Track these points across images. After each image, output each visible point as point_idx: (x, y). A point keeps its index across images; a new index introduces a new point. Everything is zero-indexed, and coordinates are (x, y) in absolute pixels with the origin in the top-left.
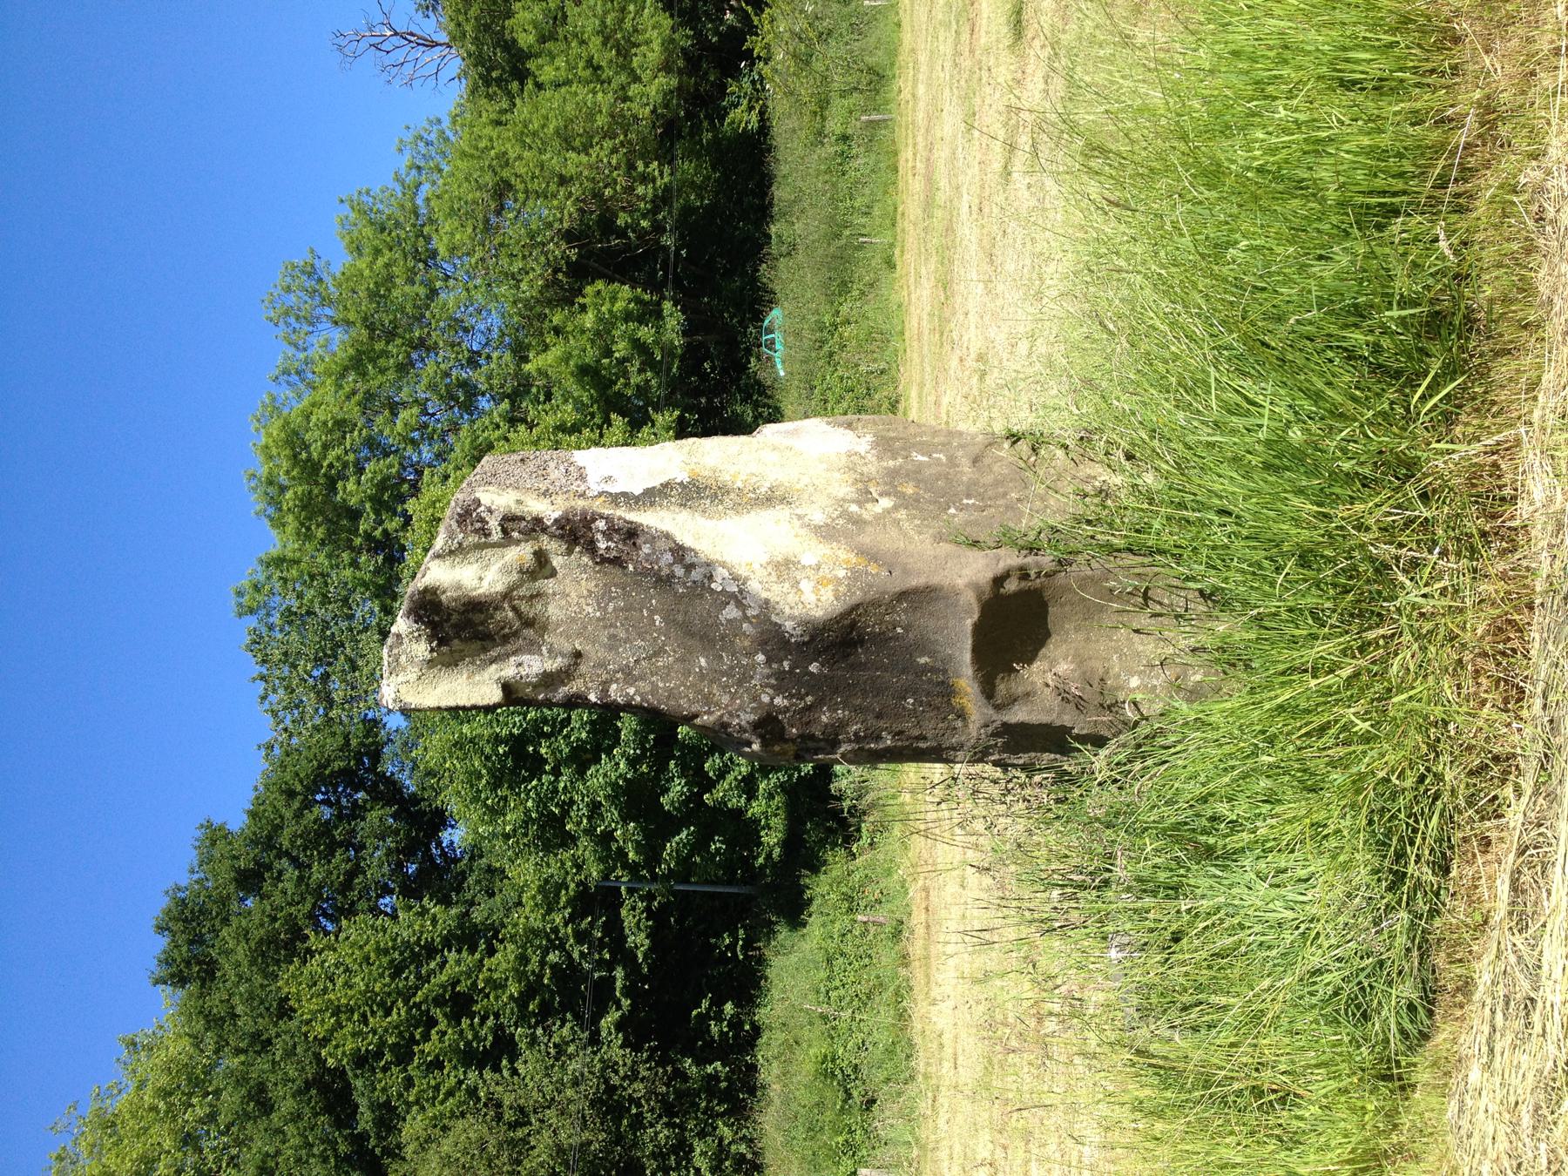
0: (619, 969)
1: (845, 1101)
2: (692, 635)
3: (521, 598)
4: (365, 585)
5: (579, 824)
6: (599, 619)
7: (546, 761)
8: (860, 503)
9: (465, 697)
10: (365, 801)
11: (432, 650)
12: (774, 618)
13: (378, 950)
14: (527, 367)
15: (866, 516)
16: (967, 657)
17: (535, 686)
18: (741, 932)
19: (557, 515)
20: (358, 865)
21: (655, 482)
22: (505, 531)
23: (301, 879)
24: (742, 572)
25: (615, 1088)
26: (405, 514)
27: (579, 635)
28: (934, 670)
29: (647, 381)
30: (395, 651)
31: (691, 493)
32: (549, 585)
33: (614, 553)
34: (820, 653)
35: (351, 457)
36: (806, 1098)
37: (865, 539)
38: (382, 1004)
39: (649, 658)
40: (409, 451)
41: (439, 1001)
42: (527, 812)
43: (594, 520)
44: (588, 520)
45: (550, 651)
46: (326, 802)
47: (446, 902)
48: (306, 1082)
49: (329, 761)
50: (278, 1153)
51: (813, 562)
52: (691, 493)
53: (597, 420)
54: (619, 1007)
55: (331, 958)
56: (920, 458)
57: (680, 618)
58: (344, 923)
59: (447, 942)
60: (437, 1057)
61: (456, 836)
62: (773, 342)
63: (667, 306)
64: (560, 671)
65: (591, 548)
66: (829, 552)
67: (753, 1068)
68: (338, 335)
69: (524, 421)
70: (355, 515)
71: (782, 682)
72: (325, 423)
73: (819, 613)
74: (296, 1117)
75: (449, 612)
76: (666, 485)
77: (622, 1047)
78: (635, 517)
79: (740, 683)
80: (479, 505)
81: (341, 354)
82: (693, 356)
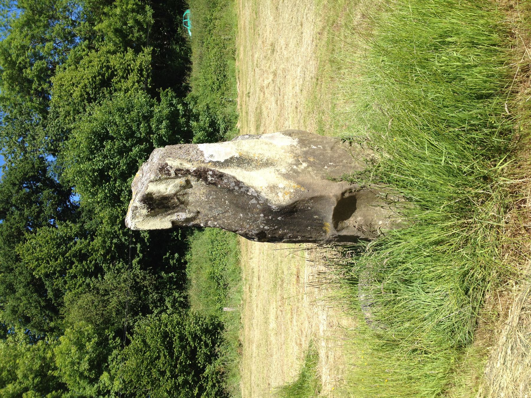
0: (139, 244)
1: (218, 286)
2: (239, 207)
3: (180, 195)
4: (36, 108)
5: (125, 198)
6: (206, 201)
7: (111, 177)
8: (297, 165)
9: (159, 226)
10: (41, 186)
11: (148, 212)
12: (269, 204)
13: (51, 239)
14: (95, 28)
15: (299, 170)
16: (331, 217)
17: (183, 222)
18: (180, 231)
19: (195, 169)
20: (41, 209)
21: (228, 157)
22: (176, 174)
23: (20, 214)
24: (259, 190)
25: (138, 283)
26: (50, 82)
27: (199, 206)
28: (319, 220)
29: (141, 36)
30: (135, 212)
31: (241, 161)
32: (189, 191)
33: (214, 182)
34: (282, 214)
35: (28, 60)
36: (204, 285)
37: (300, 179)
38: (54, 257)
39: (223, 213)
40: (50, 58)
41: (74, 256)
42: (106, 194)
43: (208, 171)
44: (206, 171)
45: (189, 211)
46: (27, 187)
47: (74, 222)
48: (28, 282)
49: (27, 173)
50: (19, 305)
51: (283, 186)
52: (241, 161)
53: (122, 49)
54: (139, 257)
55: (34, 241)
56: (314, 147)
57: (235, 202)
58: (38, 229)
59: (76, 235)
60: (75, 274)
61: (75, 198)
62: (186, 22)
63: (148, 7)
64: (192, 218)
65: (206, 179)
66: (288, 183)
67: (185, 274)
68: (20, 12)
69: (94, 48)
70: (30, 82)
71: (268, 222)
72: (17, 47)
73: (284, 204)
74: (25, 294)
75: (156, 200)
76: (231, 158)
77: (140, 269)
78: (222, 171)
79: (253, 222)
80: (167, 165)
81: (21, 20)
82: (156, 27)
